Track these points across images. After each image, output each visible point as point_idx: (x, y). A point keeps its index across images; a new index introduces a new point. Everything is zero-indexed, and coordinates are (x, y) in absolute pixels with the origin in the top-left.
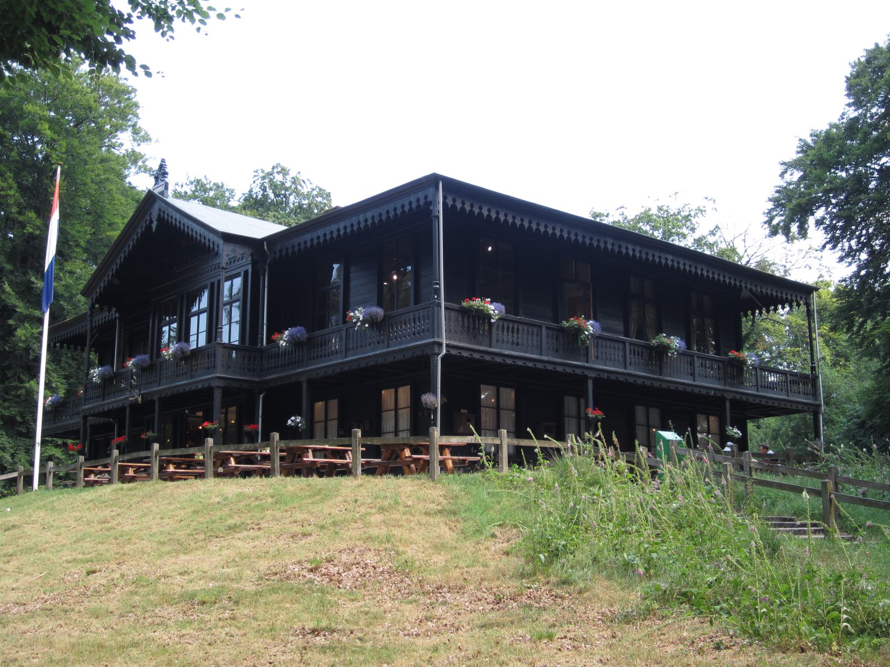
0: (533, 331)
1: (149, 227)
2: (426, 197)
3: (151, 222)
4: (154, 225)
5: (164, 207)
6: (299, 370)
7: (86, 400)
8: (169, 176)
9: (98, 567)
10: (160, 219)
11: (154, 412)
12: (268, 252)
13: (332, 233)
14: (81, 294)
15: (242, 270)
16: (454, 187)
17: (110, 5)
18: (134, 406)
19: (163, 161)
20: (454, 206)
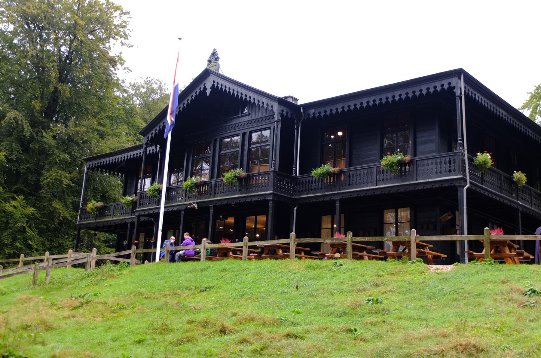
2: (450, 84)
8: (220, 60)
11: (165, 213)
12: (303, 114)
13: (124, 157)
14: (139, 134)
15: (241, 132)
16: (470, 81)
19: (215, 50)
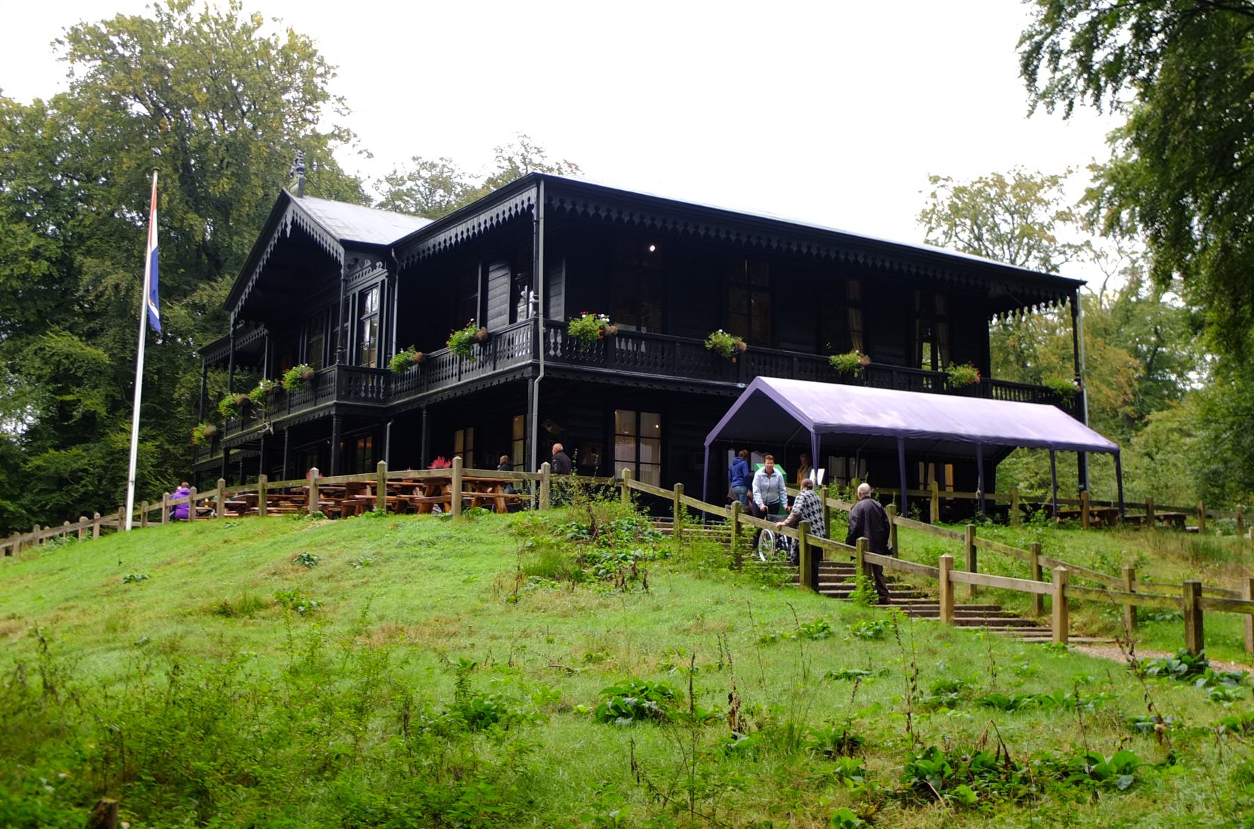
0: (663, 348)
1: (284, 232)
3: (286, 225)
4: (288, 230)
5: (297, 210)
6: (717, 383)
7: (227, 430)
9: (67, 565)
10: (294, 223)
17: (129, 18)
18: (267, 435)
20: (562, 208)
